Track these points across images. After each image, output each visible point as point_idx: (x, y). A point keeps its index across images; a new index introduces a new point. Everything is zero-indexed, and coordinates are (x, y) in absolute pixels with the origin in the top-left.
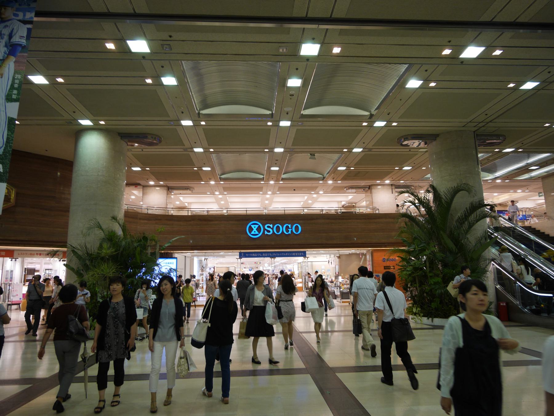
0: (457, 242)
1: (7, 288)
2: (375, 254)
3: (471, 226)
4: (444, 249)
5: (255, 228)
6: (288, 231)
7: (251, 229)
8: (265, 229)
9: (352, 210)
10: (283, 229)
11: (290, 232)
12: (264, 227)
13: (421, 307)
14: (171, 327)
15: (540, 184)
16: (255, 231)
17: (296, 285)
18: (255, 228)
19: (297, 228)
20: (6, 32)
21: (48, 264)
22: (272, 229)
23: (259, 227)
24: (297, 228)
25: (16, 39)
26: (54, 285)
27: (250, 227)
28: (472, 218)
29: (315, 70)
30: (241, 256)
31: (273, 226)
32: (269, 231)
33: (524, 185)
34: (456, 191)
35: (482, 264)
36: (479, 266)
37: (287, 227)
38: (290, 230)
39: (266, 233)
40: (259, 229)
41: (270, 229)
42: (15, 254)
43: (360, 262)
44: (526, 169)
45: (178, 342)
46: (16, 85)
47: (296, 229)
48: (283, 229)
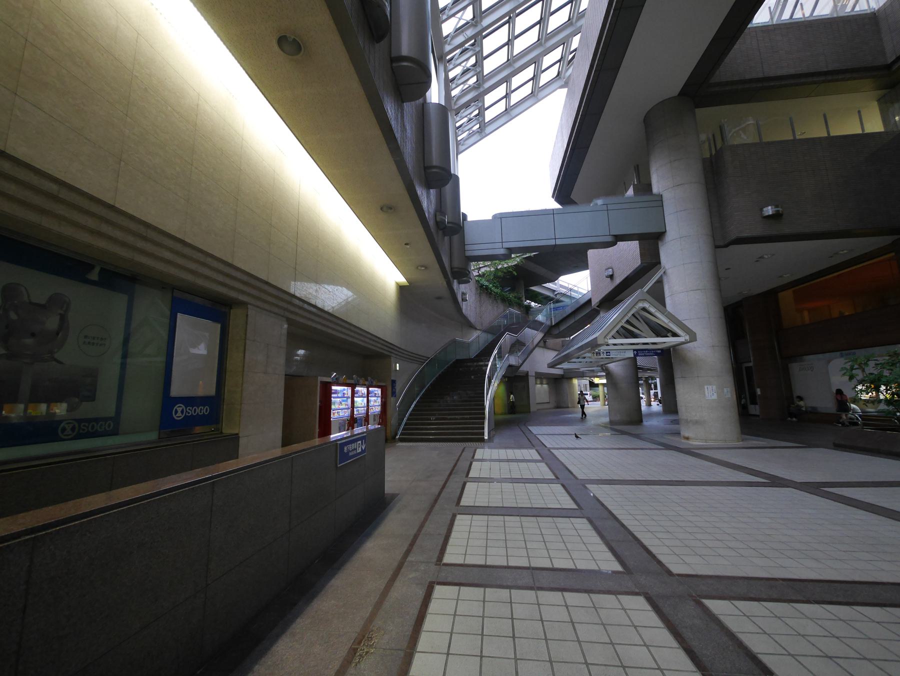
1: (360, 431)
6: (201, 412)
7: (176, 412)
11: (202, 413)
12: (186, 410)
14: (356, 632)
16: (179, 414)
17: (874, 9)
21: (374, 420)
23: (183, 410)
27: (176, 409)
29: (415, 403)
31: (192, 409)
32: (189, 413)
37: (201, 409)
38: (202, 411)
40: (182, 412)
43: (365, 455)
45: (402, 110)
46: (360, 402)
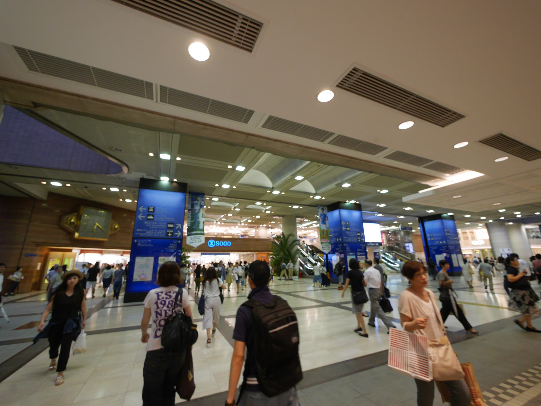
0: (289, 252)
2: (258, 255)
3: (293, 247)
4: (285, 254)
5: (212, 243)
6: (225, 244)
7: (210, 243)
8: (216, 244)
9: (254, 238)
10: (223, 244)
13: (277, 273)
15: (316, 229)
18: (212, 243)
19: (229, 244)
20: (199, 203)
22: (219, 243)
24: (229, 244)
25: (202, 204)
26: (475, 259)
28: (294, 244)
30: (202, 254)
33: (312, 229)
34: (289, 236)
35: (295, 259)
36: (412, 349)
37: (225, 243)
39: (216, 245)
40: (213, 243)
41: (218, 243)
42: (103, 252)
44: (311, 225)
47: (228, 244)
48: (223, 244)
